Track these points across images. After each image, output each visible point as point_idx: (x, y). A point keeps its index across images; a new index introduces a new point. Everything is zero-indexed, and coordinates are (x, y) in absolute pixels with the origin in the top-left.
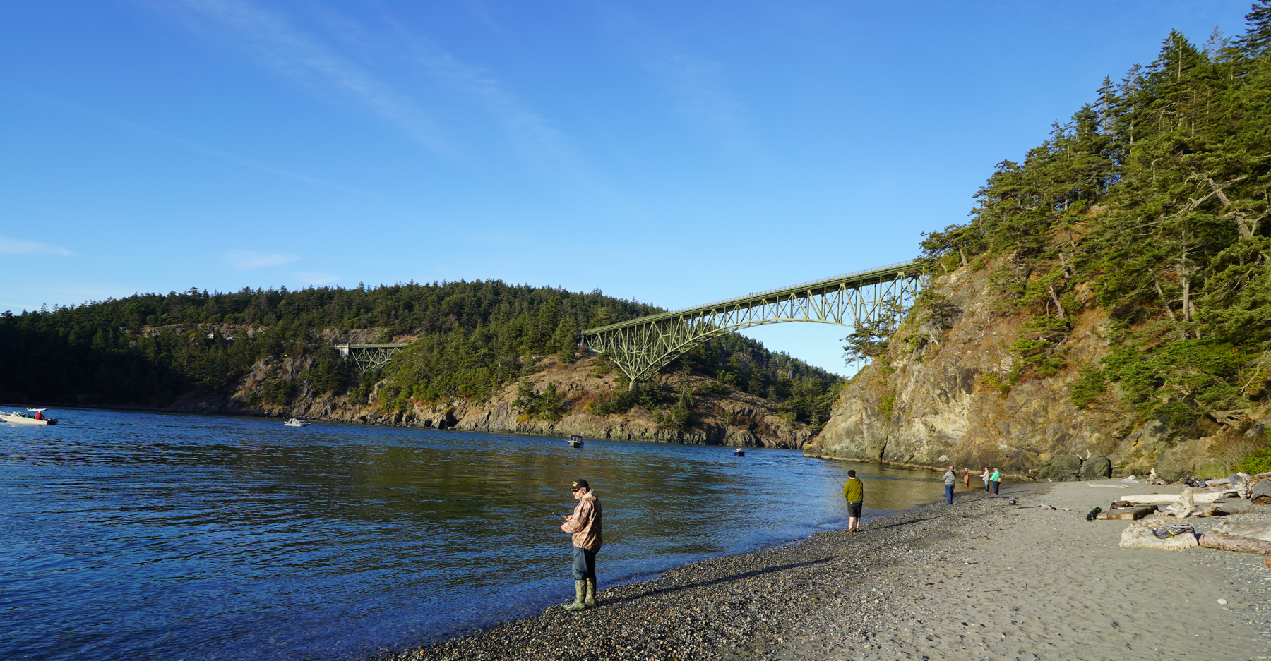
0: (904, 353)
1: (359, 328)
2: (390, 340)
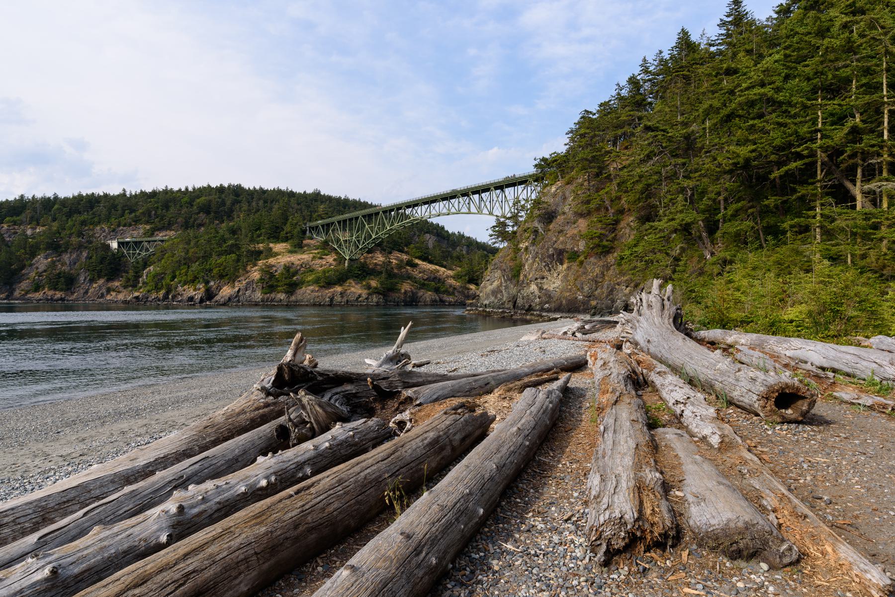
1: (124, 226)
2: (152, 235)
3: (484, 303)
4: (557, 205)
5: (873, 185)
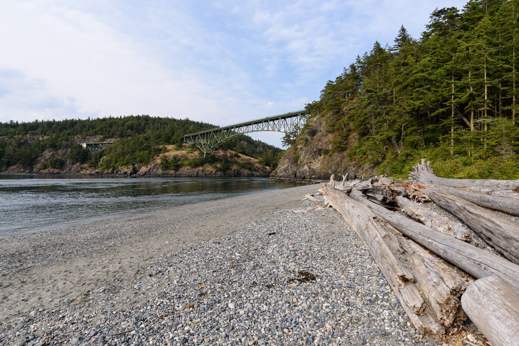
0: (301, 143)
1: (90, 136)
2: (104, 141)
3: (280, 175)
4: (317, 127)
5: (481, 120)
